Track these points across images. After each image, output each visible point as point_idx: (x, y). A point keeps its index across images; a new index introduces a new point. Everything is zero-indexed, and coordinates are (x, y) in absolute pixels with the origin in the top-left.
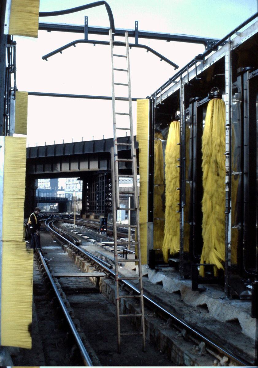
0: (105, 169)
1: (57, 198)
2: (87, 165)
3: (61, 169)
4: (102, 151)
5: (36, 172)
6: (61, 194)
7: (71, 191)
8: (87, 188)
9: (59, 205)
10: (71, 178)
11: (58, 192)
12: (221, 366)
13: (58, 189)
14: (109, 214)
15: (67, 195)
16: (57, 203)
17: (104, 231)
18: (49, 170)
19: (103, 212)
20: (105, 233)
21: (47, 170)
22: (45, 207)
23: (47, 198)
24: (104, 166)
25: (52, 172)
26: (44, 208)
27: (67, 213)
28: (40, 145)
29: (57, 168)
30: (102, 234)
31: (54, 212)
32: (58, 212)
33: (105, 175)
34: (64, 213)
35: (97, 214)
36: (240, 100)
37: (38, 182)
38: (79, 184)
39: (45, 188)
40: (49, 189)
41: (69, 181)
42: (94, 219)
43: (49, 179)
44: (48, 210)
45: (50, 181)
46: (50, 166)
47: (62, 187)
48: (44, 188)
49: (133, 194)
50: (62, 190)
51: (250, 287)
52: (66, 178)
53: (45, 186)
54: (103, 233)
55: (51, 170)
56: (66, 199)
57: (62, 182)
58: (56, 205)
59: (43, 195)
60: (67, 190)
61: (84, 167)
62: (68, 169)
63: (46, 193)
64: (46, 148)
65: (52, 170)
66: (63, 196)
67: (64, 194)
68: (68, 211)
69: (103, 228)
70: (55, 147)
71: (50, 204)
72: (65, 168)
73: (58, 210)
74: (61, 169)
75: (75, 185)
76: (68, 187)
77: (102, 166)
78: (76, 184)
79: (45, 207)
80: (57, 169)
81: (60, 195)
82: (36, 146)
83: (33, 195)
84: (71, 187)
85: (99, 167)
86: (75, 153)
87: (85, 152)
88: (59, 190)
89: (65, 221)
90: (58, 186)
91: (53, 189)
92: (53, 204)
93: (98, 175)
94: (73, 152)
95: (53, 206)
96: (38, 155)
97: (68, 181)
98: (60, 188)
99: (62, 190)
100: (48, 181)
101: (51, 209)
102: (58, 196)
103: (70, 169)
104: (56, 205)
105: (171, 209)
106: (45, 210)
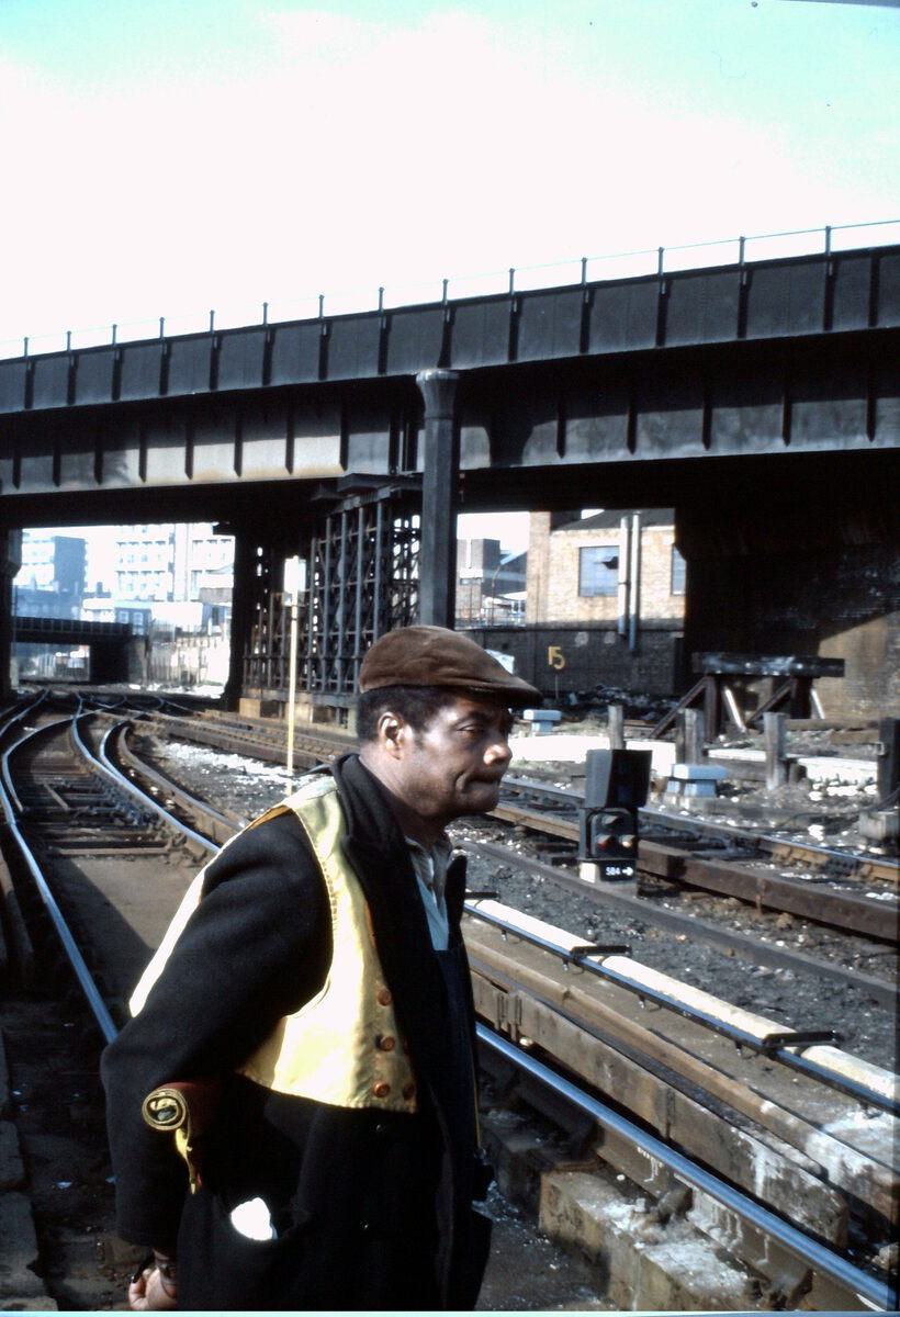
0: (381, 468)
1: (78, 623)
3: (143, 473)
4: (371, 373)
5: (17, 483)
6: (99, 611)
8: (256, 572)
9: (92, 652)
11: (87, 603)
13: (86, 590)
15: (124, 615)
16: (84, 643)
18: (82, 478)
20: (629, 871)
21: (74, 478)
22: (36, 661)
23: (47, 621)
24: (372, 456)
25: (95, 487)
26: (33, 663)
27: (135, 687)
29: (125, 467)
30: (603, 876)
31: (71, 678)
32: (87, 679)
34: (118, 688)
36: (40, 605)
39: (36, 586)
40: (50, 589)
42: (312, 726)
44: (49, 672)
46: (91, 458)
47: (100, 585)
48: (32, 588)
50: (101, 593)
51: (857, 956)
53: (34, 580)
54: (612, 871)
55: (91, 474)
56: (128, 628)
58: (81, 653)
61: (264, 459)
63: (40, 605)
65: (99, 478)
66: (108, 618)
67: (110, 611)
71: (56, 646)
73: (88, 672)
74: (143, 473)
77: (361, 456)
79: (36, 661)
80: (121, 469)
86: (222, 388)
88: (90, 596)
89: (176, 733)
90: (86, 579)
91: (65, 590)
92: (67, 646)
93: (337, 503)
94: (213, 382)
95: (69, 657)
98: (91, 588)
99: (101, 593)
101: (62, 668)
103: (189, 470)
104: (81, 653)
105: (434, 661)
106: (34, 673)
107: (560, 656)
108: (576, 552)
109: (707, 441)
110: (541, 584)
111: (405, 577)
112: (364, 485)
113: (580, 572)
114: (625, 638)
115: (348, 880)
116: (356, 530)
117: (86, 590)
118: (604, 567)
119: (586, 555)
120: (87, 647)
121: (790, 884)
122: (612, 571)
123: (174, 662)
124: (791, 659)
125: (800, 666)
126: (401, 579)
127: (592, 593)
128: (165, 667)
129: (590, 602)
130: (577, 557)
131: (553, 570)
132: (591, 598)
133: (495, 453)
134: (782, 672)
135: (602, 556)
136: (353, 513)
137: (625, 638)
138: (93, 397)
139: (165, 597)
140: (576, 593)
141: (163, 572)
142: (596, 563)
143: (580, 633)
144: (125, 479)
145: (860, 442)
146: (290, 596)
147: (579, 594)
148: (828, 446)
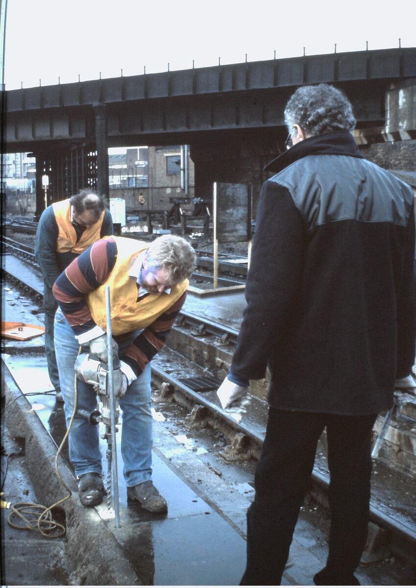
38: (14, 165)
85: (70, 133)
108: (165, 158)
109: (188, 127)
110: (153, 170)
111: (94, 173)
113: (167, 165)
114: (184, 190)
115: (235, 421)
116: (76, 157)
118: (175, 164)
119: (169, 159)
121: (241, 283)
122: (178, 165)
123: (17, 204)
124: (199, 198)
125: (202, 200)
126: (93, 174)
127: (171, 174)
129: (171, 177)
130: (165, 160)
131: (157, 165)
132: (171, 175)
133: (193, 92)
134: (197, 203)
135: (175, 160)
136: (74, 151)
137: (184, 190)
139: (12, 176)
140: (166, 174)
141: (11, 165)
142: (173, 162)
143: (168, 189)
146: (44, 186)
147: (167, 174)
148: (225, 127)
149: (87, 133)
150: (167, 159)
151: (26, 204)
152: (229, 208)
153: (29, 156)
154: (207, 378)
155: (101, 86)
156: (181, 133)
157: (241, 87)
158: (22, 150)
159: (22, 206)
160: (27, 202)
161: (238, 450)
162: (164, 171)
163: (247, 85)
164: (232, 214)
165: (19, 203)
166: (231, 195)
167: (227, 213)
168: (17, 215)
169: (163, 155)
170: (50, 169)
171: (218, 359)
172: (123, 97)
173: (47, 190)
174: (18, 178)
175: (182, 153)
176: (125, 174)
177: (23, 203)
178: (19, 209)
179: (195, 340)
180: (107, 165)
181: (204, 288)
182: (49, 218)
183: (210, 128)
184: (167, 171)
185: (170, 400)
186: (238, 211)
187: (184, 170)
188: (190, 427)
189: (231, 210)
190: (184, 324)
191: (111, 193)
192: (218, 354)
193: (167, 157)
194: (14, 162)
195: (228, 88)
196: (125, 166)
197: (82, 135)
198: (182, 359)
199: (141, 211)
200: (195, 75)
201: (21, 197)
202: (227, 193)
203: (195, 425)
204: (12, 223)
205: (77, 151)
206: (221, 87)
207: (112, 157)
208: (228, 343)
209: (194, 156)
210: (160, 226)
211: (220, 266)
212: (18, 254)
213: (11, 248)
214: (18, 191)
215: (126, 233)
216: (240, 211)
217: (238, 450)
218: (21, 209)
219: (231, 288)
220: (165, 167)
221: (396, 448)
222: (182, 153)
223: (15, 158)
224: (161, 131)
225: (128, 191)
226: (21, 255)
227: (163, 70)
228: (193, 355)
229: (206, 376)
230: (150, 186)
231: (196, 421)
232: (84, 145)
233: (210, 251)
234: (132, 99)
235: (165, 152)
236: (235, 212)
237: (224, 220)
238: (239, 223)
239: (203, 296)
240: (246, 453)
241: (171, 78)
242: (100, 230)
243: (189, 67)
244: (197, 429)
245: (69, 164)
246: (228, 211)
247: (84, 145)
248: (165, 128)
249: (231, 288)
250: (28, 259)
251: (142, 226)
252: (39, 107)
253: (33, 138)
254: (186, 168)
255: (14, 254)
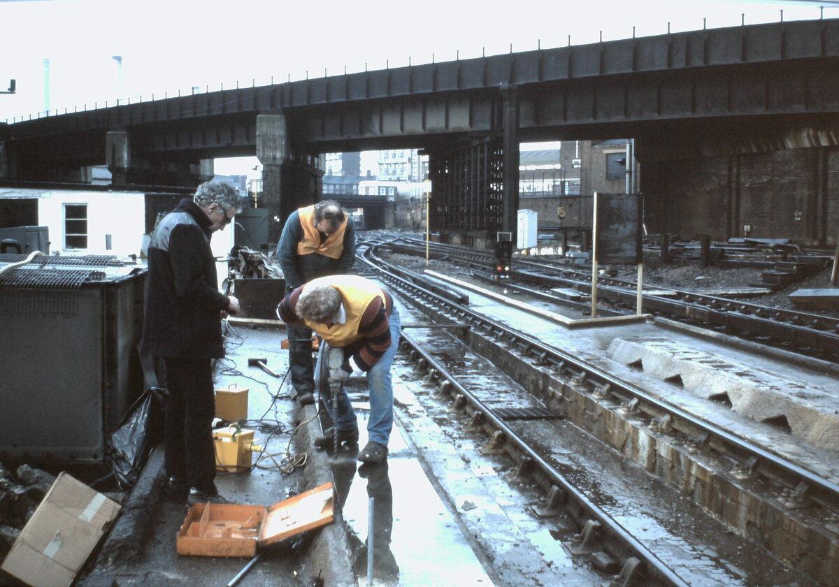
0: (487, 127)
2: (399, 123)
3: (381, 130)
7: (390, 180)
9: (365, 212)
10: (397, 150)
12: (784, 583)
13: (361, 175)
14: (510, 233)
16: (360, 207)
17: (505, 273)
19: (481, 229)
28: (295, 79)
29: (373, 127)
33: (487, 143)
35: (446, 232)
37: (325, 160)
38: (410, 164)
41: (394, 156)
43: (341, 153)
45: (343, 159)
47: (369, 172)
49: (379, 187)
52: (378, 151)
56: (384, 199)
57: (370, 159)
58: (359, 213)
59: (328, 190)
60: (383, 177)
62: (421, 126)
64: (540, 57)
65: (361, 133)
66: (373, 192)
68: (387, 226)
69: (503, 265)
70: (368, 79)
72: (392, 127)
74: (381, 130)
75: (399, 167)
76: (383, 172)
78: (403, 163)
80: (371, 128)
81: (365, 189)
82: (480, 56)
83: (316, 190)
84: (390, 172)
85: (471, 124)
87: (714, 62)
96: (328, 97)
97: (383, 157)
98: (363, 174)
100: (338, 158)
102: (362, 192)
103: (402, 129)
104: (359, 213)
107: (563, 212)
109: (626, 114)
112: (481, 135)
117: (361, 175)
119: (610, 158)
120: (362, 210)
128: (403, 219)
138: (359, 96)
140: (605, 177)
144: (373, 133)
145: (689, 115)
148: (676, 116)
149: (492, 125)
150: (607, 159)
151: (419, 217)
152: (613, 224)
153: (420, 153)
154: (538, 409)
155: (513, 62)
156: (586, 125)
157: (698, 62)
158: (411, 146)
159: (415, 218)
160: (422, 214)
161: (494, 445)
162: (602, 174)
163: (706, 59)
164: (617, 230)
165: (411, 214)
166: (617, 207)
167: (611, 229)
168: (407, 231)
169: (602, 152)
170: (447, 171)
171: (551, 388)
172: (540, 75)
173: (429, 198)
174: (415, 181)
175: (626, 148)
176: (558, 178)
177: (417, 215)
178: (410, 223)
179: (533, 369)
180: (517, 163)
181: (572, 318)
182: (295, 221)
183: (656, 117)
184: (607, 174)
185: (462, 412)
186: (625, 227)
187: (630, 172)
188: (466, 431)
189: (616, 225)
190: (530, 353)
191: (521, 203)
192: (551, 382)
193: (607, 155)
194: (410, 160)
195: (680, 64)
196: (558, 166)
197: (487, 127)
198: (521, 391)
199: (570, 228)
200: (636, 46)
201: (414, 207)
202: (611, 205)
203: (471, 429)
204: (396, 241)
205: (479, 148)
206: (670, 60)
207: (523, 153)
208: (563, 372)
209: (639, 155)
210: (577, 247)
211: (646, 300)
212: (384, 278)
213: (379, 270)
214: (412, 199)
215: (536, 256)
216: (628, 227)
217: (494, 445)
218: (414, 223)
219: (608, 319)
220: (605, 168)
221: (670, 465)
222: (626, 148)
223: (412, 154)
224: (591, 120)
225: (553, 200)
226: (387, 279)
227: (593, 39)
228: (531, 387)
229: (538, 407)
230: (583, 193)
231: (473, 426)
232: (487, 139)
233: (631, 281)
234: (552, 79)
235: (606, 148)
236: (621, 228)
237: (607, 237)
238: (627, 242)
239: (572, 327)
240: (501, 448)
241: (603, 51)
242: (343, 233)
243: (628, 36)
244: (472, 433)
245: (469, 165)
246: (612, 227)
247: (487, 139)
248: (595, 116)
249: (608, 319)
250: (394, 283)
251: (556, 247)
252: (431, 91)
253: (423, 131)
254: (633, 169)
255: (380, 277)
